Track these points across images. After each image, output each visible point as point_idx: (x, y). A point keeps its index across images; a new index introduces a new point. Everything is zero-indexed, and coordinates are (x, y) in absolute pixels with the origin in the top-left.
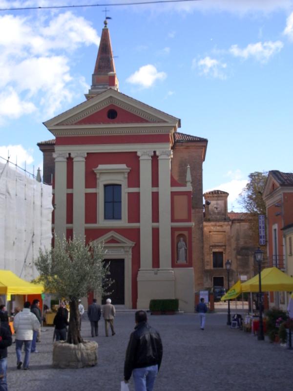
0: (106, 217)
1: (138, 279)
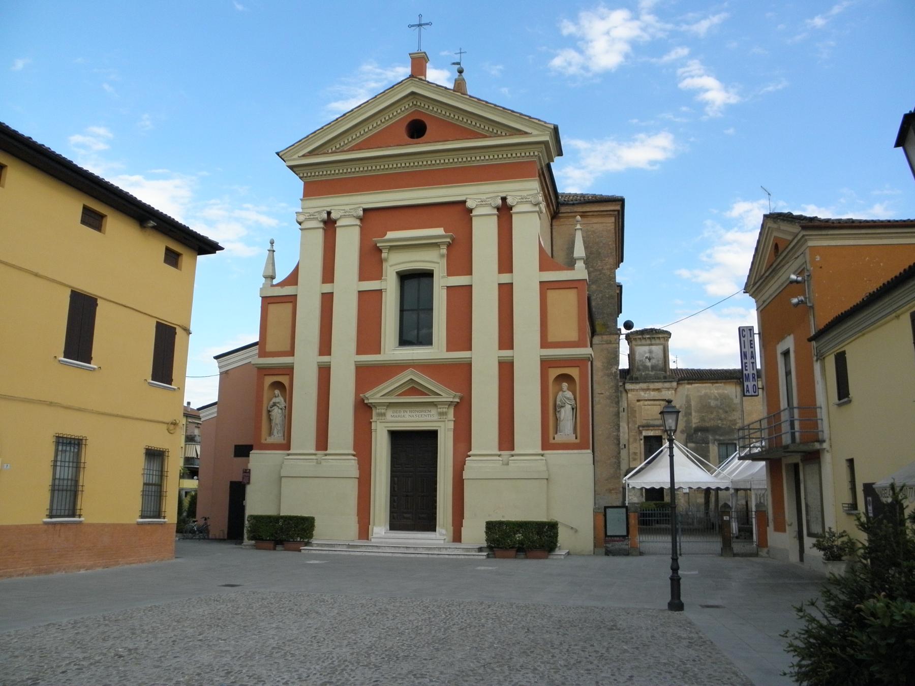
0: (404, 341)
1: (466, 475)
